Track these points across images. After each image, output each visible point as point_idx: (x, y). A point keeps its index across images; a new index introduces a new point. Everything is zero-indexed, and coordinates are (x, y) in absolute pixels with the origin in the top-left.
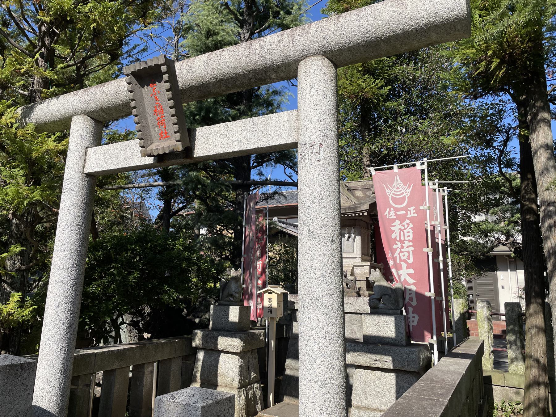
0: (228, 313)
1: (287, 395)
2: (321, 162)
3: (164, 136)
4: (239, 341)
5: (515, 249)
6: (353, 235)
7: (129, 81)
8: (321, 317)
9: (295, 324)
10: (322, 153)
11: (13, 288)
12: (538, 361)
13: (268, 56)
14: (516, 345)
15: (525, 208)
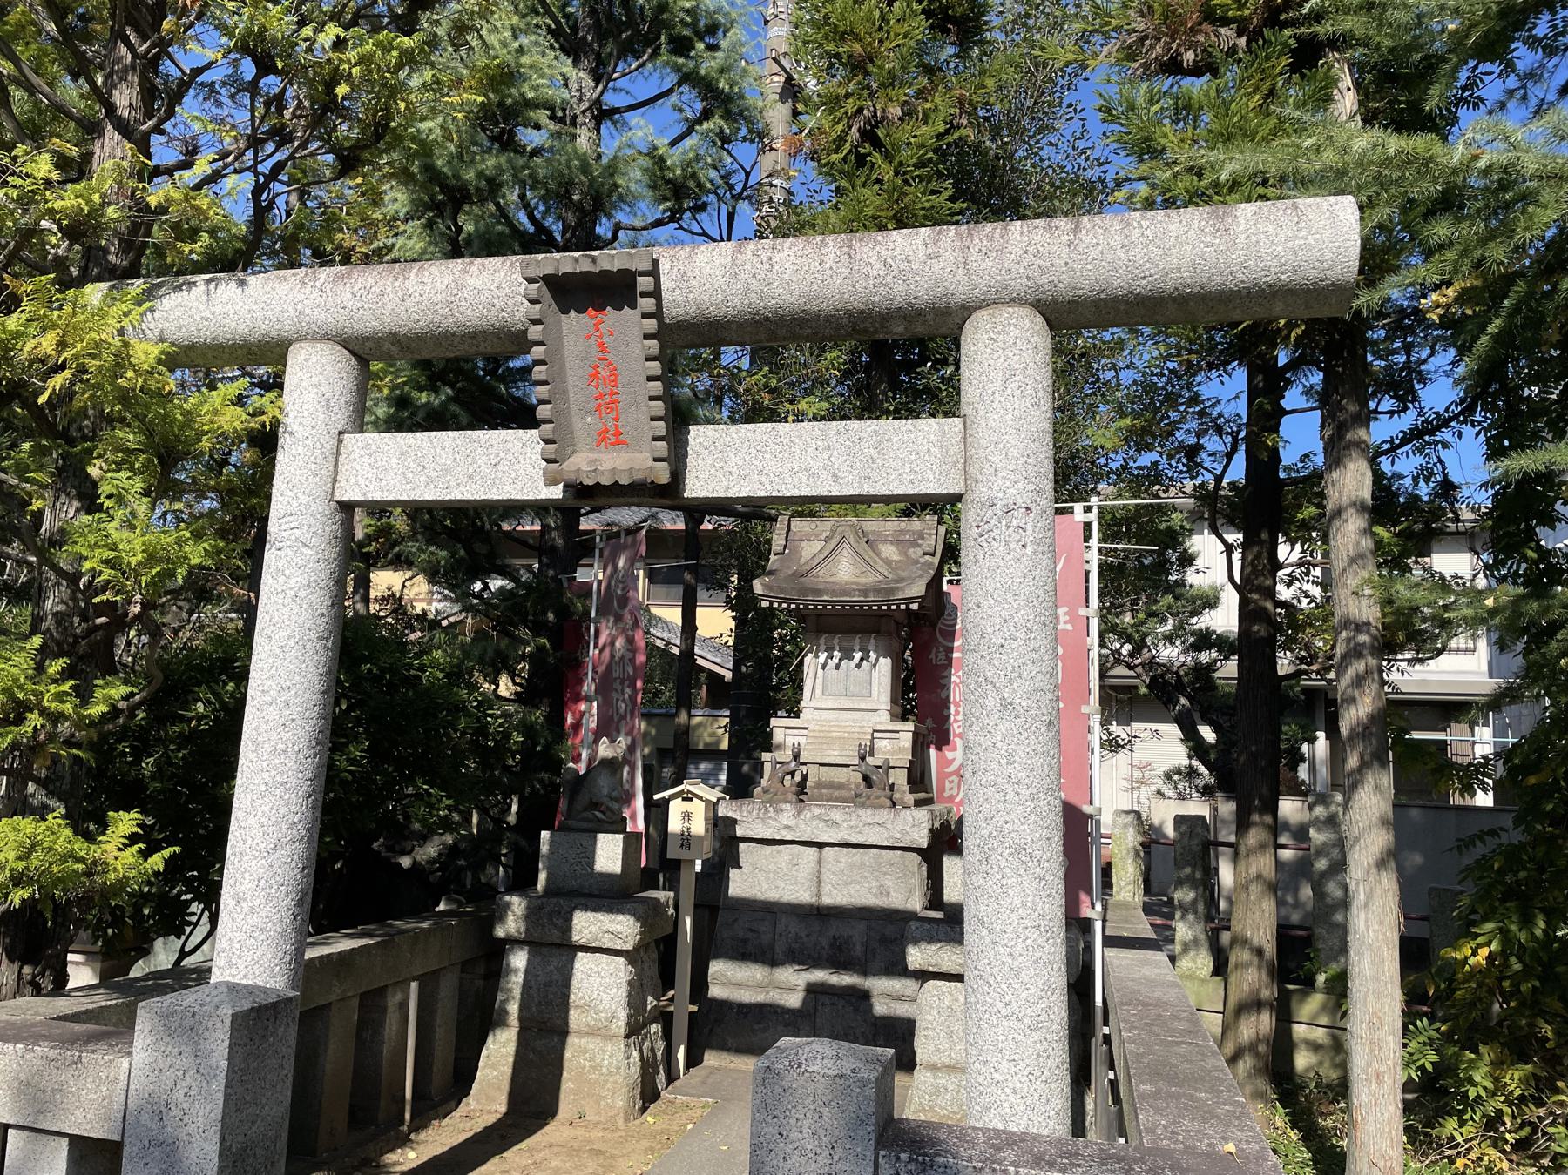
0: (594, 852)
1: (712, 1047)
2: (1029, 549)
3: (612, 438)
4: (632, 920)
5: (1153, 679)
6: (873, 655)
7: (534, 295)
8: (1030, 885)
9: (733, 873)
10: (1029, 528)
11: (51, 794)
12: (1259, 952)
13: (899, 287)
14: (1196, 912)
15: (1252, 606)
